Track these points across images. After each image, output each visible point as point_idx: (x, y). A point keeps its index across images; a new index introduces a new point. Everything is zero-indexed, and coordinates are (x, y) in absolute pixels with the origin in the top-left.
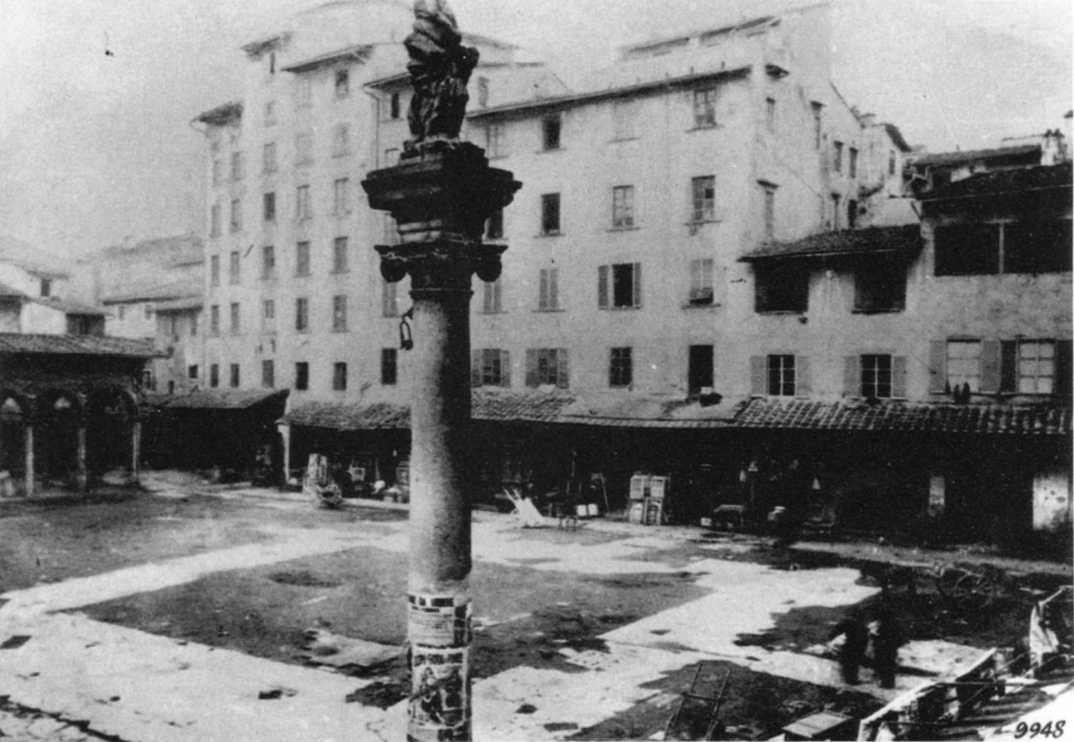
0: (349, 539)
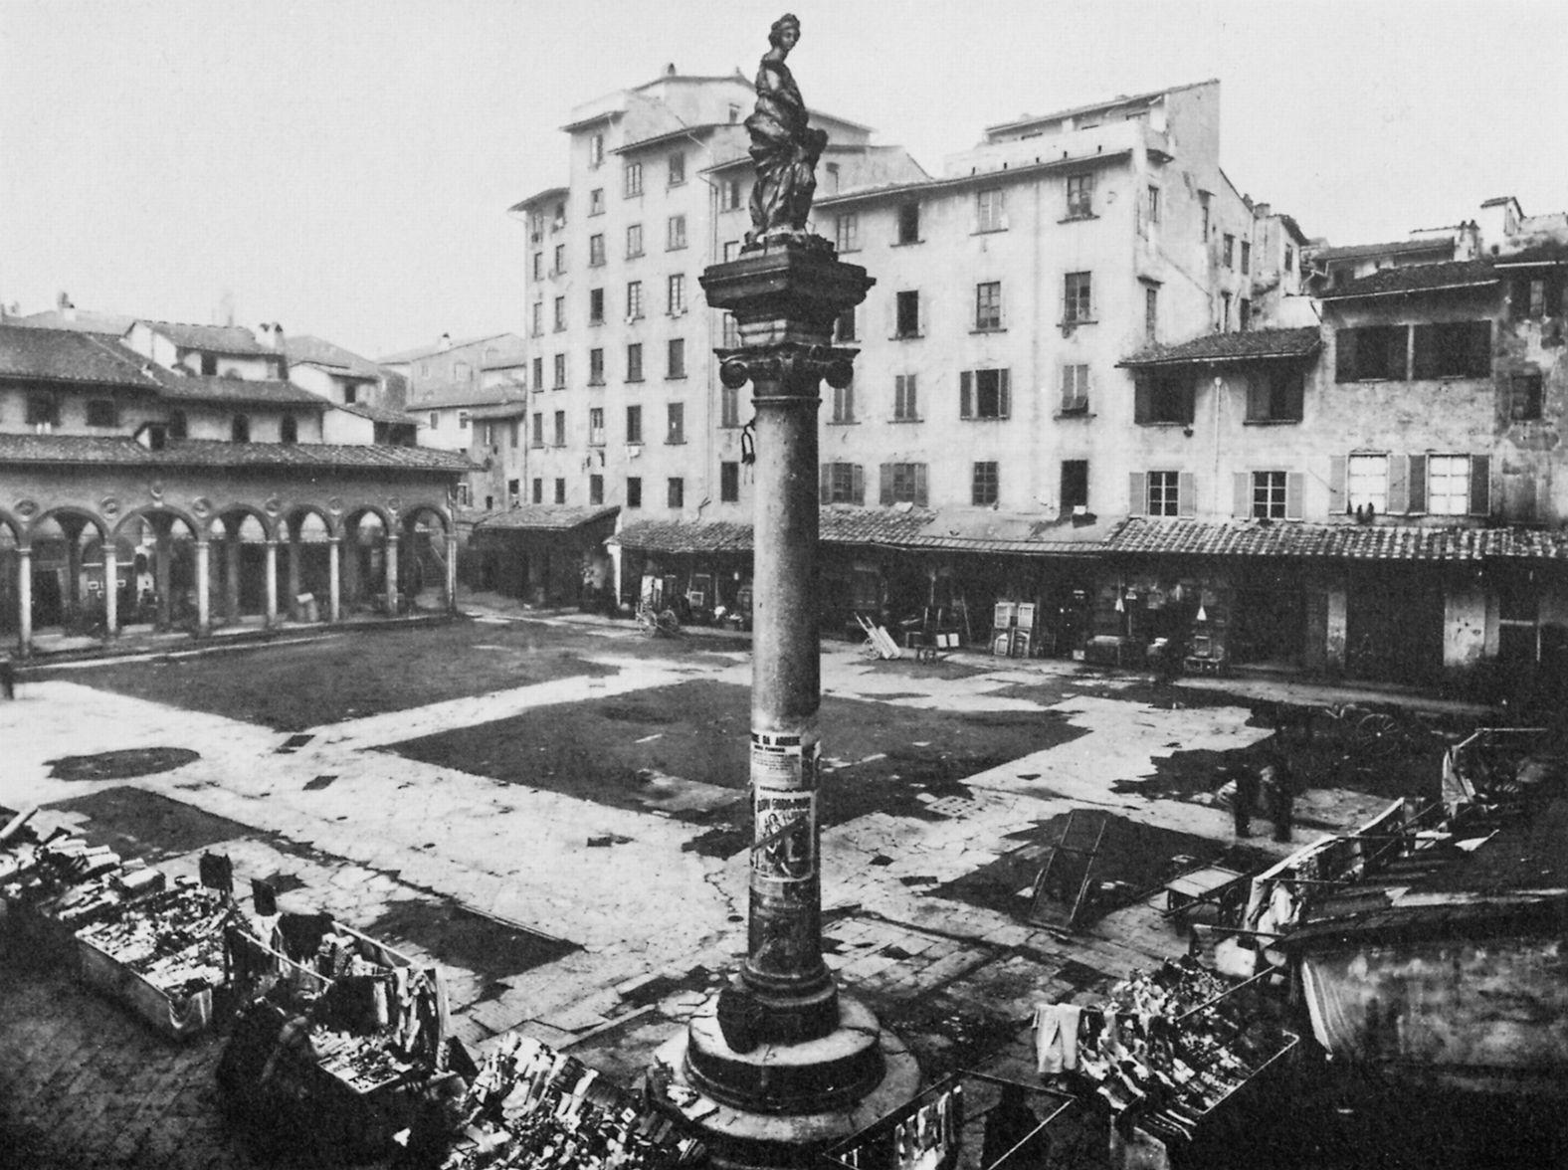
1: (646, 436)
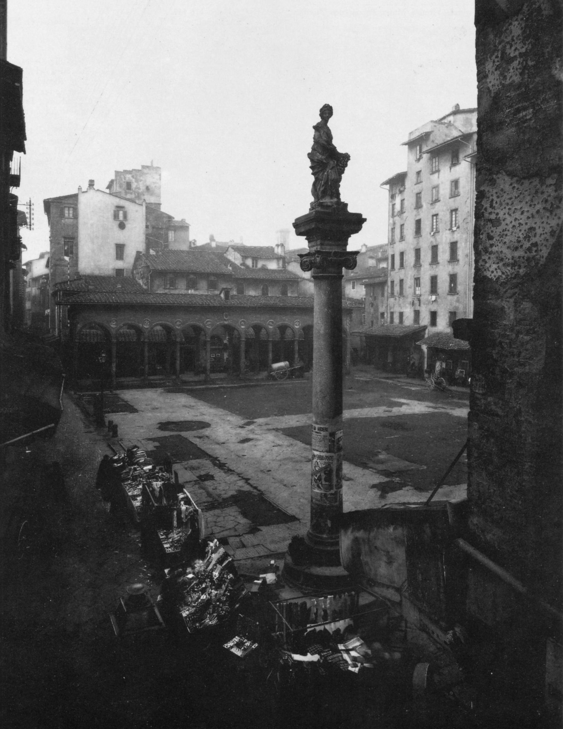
0: (436, 408)
1: (440, 291)
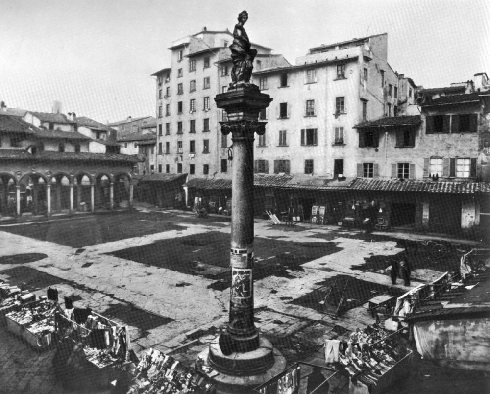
0: (209, 229)
1: (196, 151)
